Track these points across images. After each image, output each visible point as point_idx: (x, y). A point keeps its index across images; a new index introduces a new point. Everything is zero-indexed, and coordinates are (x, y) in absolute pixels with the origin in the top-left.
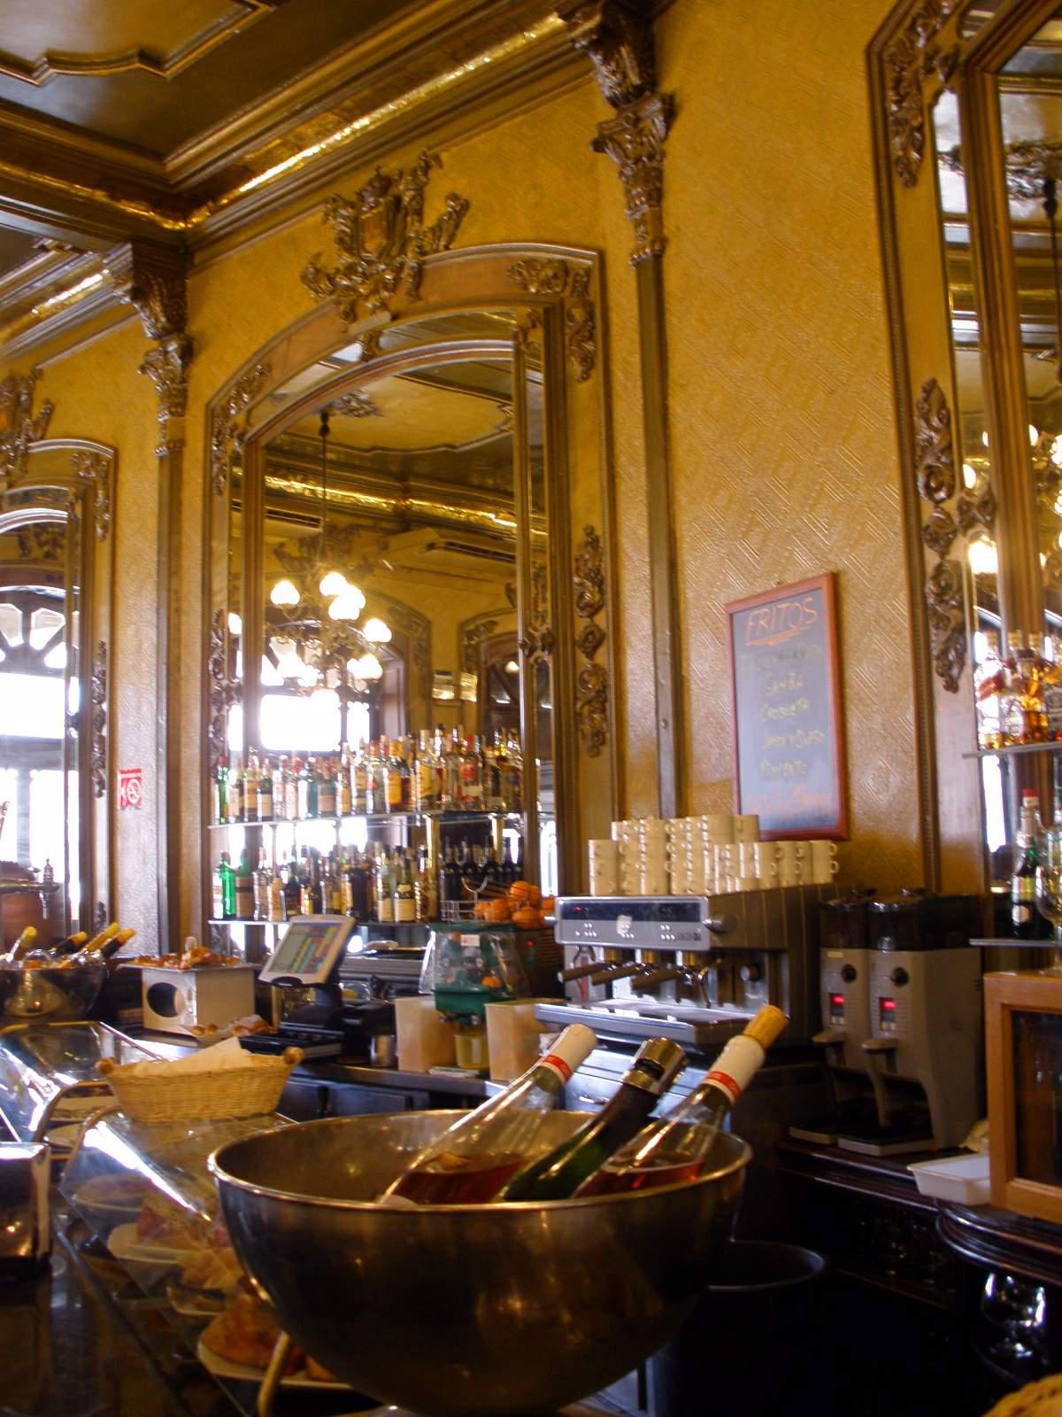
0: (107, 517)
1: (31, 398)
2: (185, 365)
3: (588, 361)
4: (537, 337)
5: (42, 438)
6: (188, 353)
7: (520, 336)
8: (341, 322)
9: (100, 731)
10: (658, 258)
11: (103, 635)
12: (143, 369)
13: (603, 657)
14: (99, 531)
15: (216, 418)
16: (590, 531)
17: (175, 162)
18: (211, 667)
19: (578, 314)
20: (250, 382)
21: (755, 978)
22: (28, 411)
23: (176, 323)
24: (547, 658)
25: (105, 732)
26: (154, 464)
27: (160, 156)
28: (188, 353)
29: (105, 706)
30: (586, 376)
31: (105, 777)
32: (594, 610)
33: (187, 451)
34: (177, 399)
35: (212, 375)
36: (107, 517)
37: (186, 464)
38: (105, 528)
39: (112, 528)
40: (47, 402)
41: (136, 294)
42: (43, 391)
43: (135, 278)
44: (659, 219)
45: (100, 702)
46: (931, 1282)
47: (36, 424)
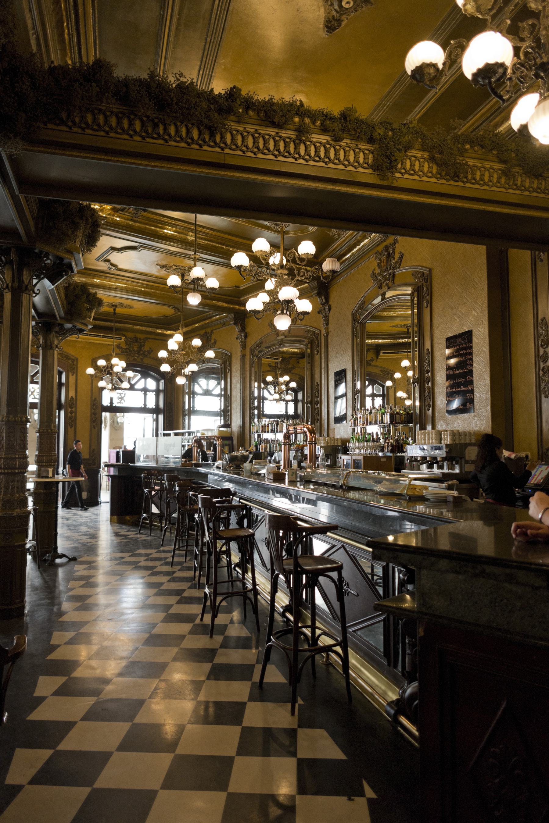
0: (428, 298)
1: (211, 338)
2: (245, 339)
3: (318, 351)
4: (309, 346)
5: (399, 268)
6: (246, 336)
7: (306, 345)
8: (276, 336)
9: (428, 384)
10: (327, 336)
11: (428, 346)
12: (237, 339)
13: (319, 406)
14: (425, 304)
15: (252, 351)
16: (317, 383)
17: (242, 299)
18: (540, 343)
19: (316, 343)
20: (258, 345)
21: (456, 464)
22: (210, 341)
23: (243, 329)
24: (309, 405)
25: (430, 384)
26: (239, 358)
27: (239, 298)
28: (246, 336)
29: (430, 374)
30: (317, 354)
31: (431, 403)
32: (318, 397)
33: (246, 357)
34: (244, 346)
35: (252, 342)
36: (428, 298)
37: (246, 360)
38: (427, 302)
39: (231, 370)
40: (215, 339)
41: (235, 324)
42: (213, 337)
43: (235, 321)
44: (328, 328)
45: (428, 373)
46: (244, 512)
47: (396, 263)
